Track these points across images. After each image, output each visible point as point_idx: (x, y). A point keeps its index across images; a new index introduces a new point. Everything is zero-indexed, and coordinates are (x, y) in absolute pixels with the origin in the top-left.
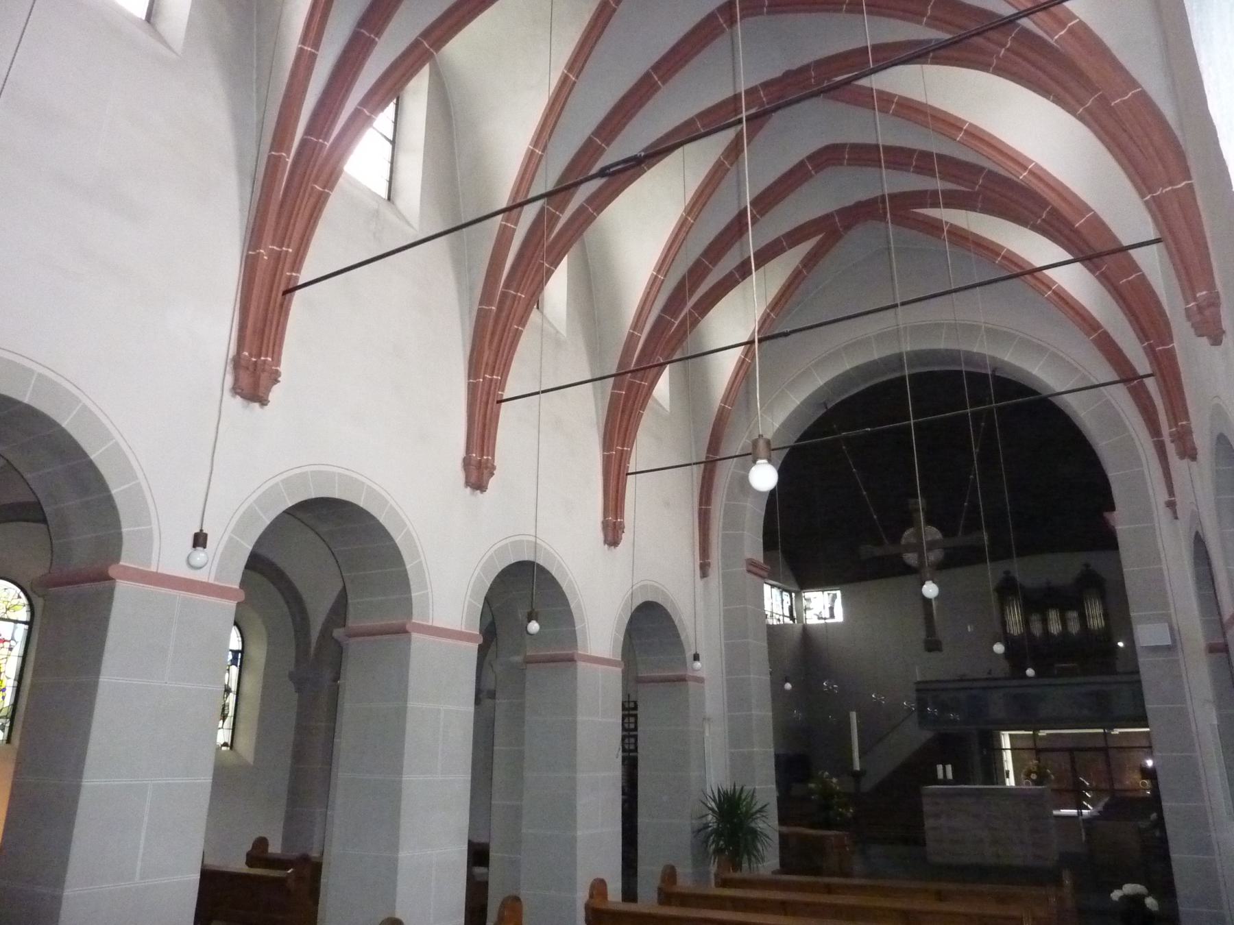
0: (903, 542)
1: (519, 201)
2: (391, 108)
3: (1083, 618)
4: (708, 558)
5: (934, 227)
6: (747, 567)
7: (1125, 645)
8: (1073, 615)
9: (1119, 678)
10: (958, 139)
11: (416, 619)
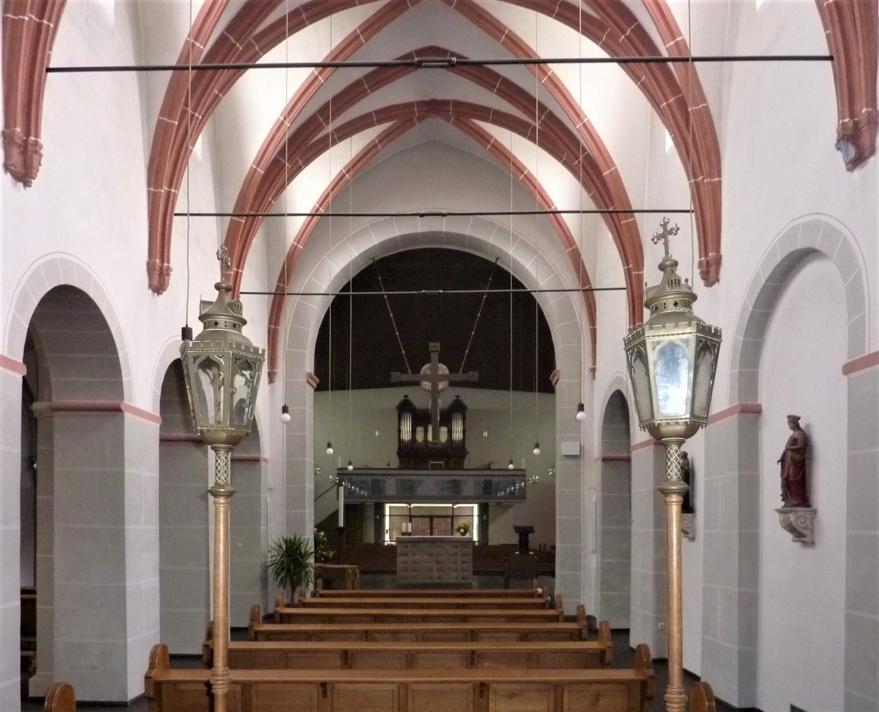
0: (422, 372)
1: (337, 62)
2: (605, 55)
3: (450, 432)
4: (275, 368)
5: (484, 138)
6: (307, 379)
7: (534, 455)
8: (444, 430)
9: (466, 473)
10: (543, 81)
11: (126, 401)
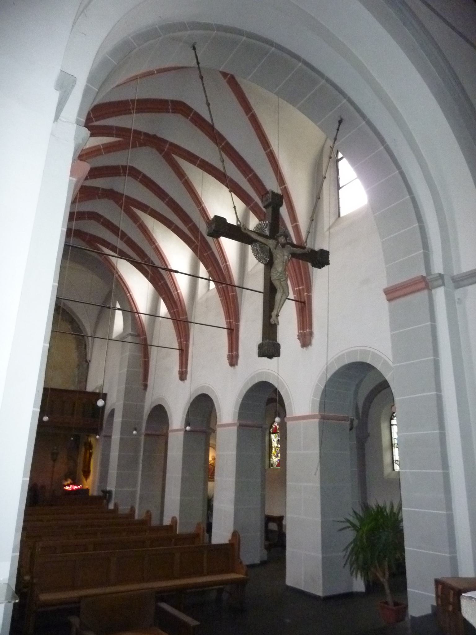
3: (69, 485)
